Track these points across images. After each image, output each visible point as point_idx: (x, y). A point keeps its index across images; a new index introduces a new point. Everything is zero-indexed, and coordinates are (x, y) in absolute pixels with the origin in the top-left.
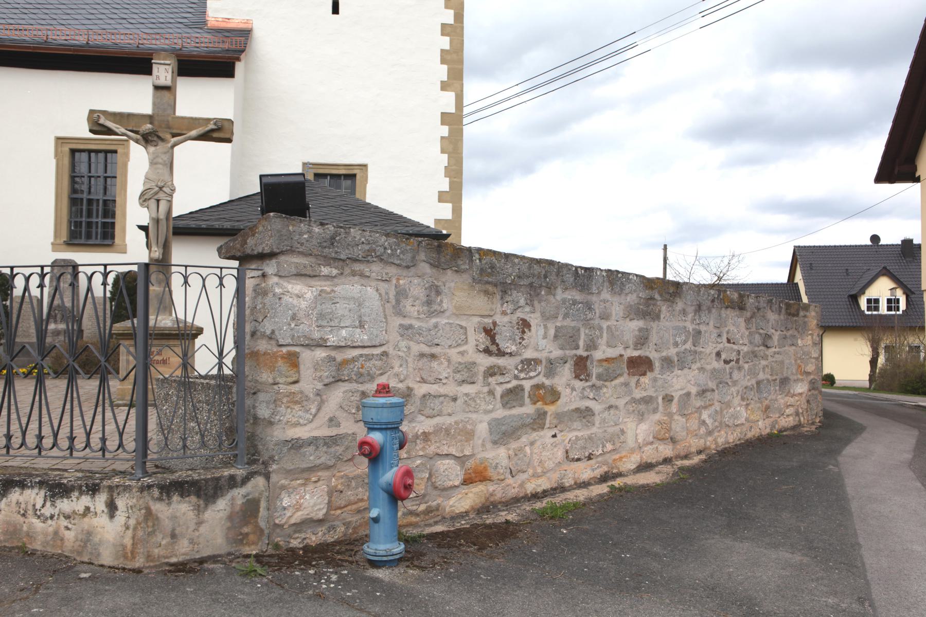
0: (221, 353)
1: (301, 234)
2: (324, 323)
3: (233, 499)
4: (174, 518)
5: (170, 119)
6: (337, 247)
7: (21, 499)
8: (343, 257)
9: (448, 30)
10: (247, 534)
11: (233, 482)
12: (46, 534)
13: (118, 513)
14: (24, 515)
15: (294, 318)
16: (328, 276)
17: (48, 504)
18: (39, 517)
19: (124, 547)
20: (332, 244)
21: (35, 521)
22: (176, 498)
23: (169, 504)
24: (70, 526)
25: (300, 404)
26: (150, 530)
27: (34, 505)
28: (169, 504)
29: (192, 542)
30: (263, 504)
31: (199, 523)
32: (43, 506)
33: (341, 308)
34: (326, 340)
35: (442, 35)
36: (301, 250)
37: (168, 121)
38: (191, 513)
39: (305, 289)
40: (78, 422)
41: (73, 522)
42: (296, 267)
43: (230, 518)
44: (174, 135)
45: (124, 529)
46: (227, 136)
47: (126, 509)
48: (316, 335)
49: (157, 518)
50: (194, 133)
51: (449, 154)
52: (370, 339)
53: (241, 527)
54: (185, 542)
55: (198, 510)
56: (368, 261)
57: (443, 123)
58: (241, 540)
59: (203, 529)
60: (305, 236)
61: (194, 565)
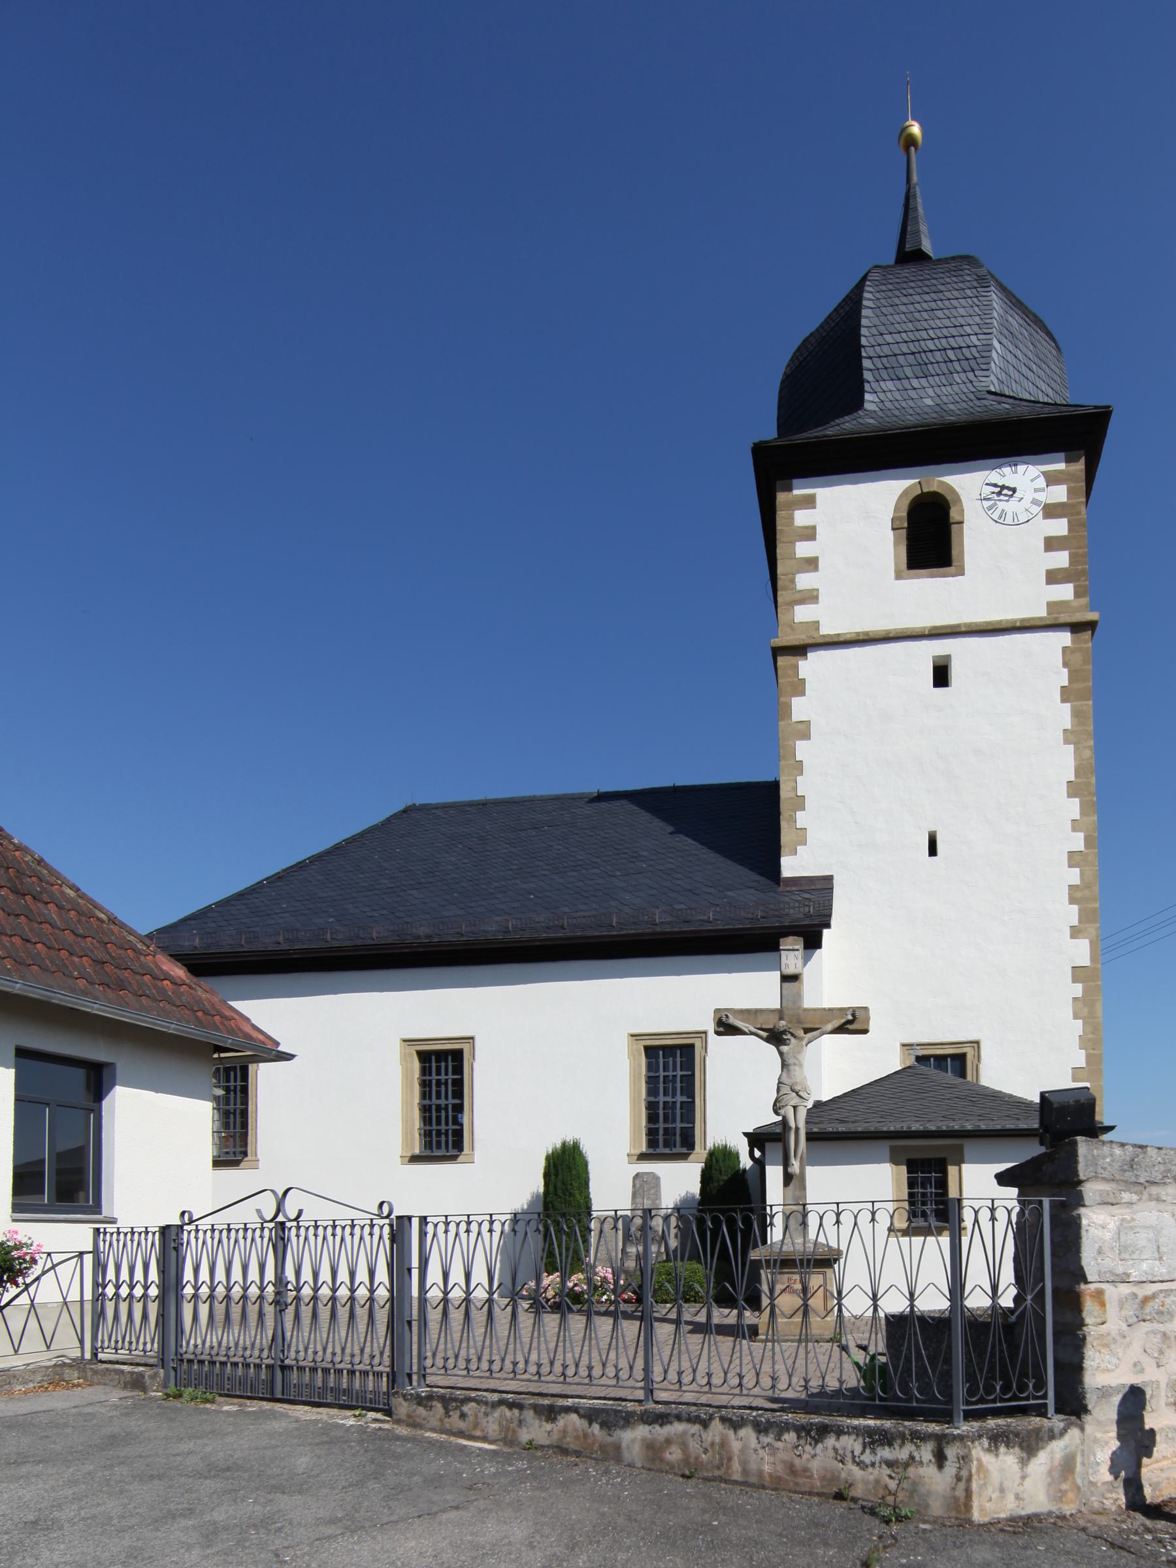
0: (995, 1288)
1: (1104, 1157)
2: (1126, 1256)
3: (1052, 1452)
4: (1002, 1470)
5: (801, 1012)
6: (1136, 1169)
7: (838, 1445)
8: (1142, 1180)
9: (1078, 858)
10: (1066, 1491)
11: (1052, 1436)
12: (866, 1482)
13: (947, 1463)
14: (842, 1462)
15: (1100, 1252)
16: (1128, 1203)
17: (868, 1451)
18: (858, 1464)
19: (956, 1499)
20: (1132, 1167)
21: (855, 1469)
22: (1002, 1449)
23: (997, 1455)
24: (893, 1475)
25: (1108, 1347)
26: (982, 1482)
27: (853, 1452)
28: (997, 1455)
29: (1018, 1497)
30: (1079, 1459)
31: (1023, 1478)
32: (862, 1454)
33: (1142, 1239)
34: (1128, 1275)
35: (1070, 866)
36: (1104, 1175)
37: (799, 1015)
38: (1016, 1465)
39: (1108, 1219)
40: (595, 1354)
41: (896, 1470)
42: (1101, 1195)
43: (1050, 1472)
44: (807, 1031)
45: (955, 1480)
46: (864, 1027)
47: (956, 1460)
48: (1120, 1270)
49: (987, 1471)
50: (829, 1027)
51: (1084, 1019)
52: (1169, 1272)
53: (1060, 1483)
54: (1010, 1497)
55: (1024, 1462)
56: (1164, 1183)
57: (1075, 980)
58: (1061, 1498)
59: (1027, 1482)
60: (1108, 1160)
61: (329, 1530)
